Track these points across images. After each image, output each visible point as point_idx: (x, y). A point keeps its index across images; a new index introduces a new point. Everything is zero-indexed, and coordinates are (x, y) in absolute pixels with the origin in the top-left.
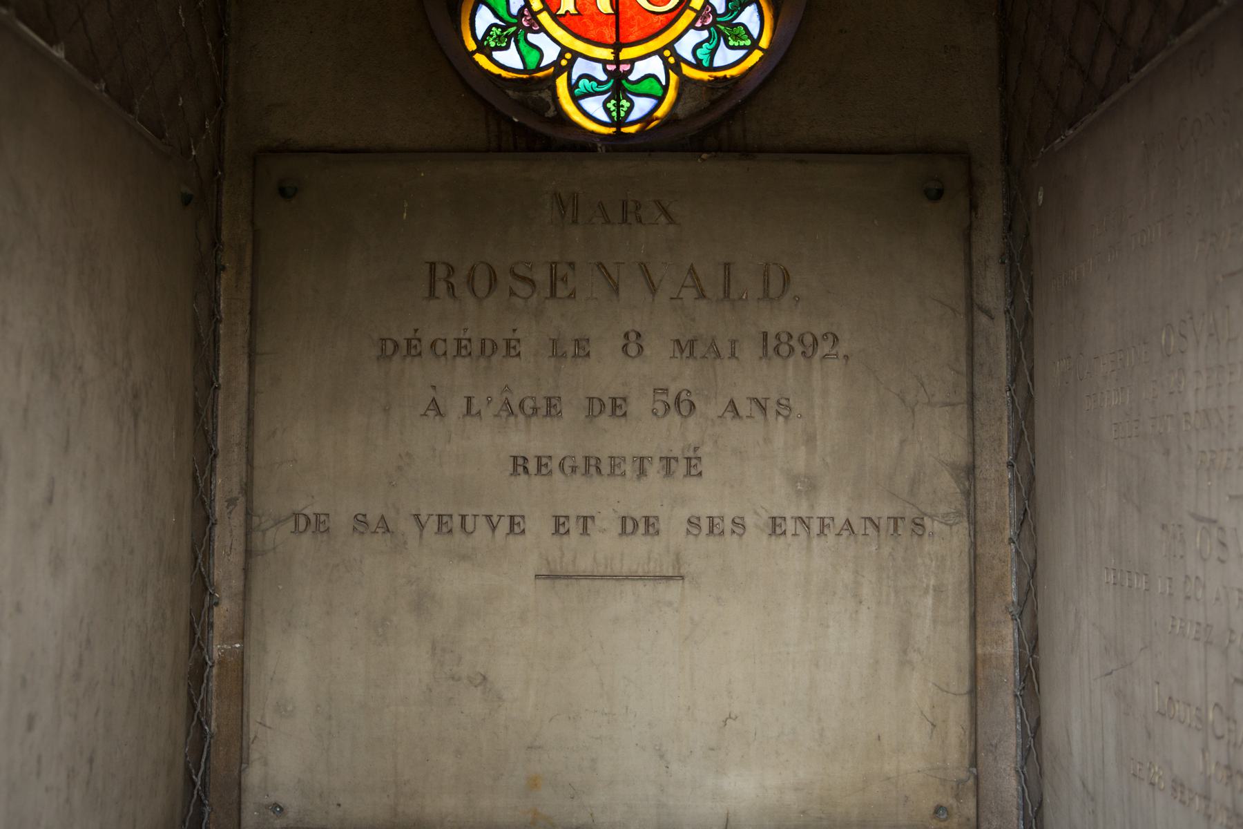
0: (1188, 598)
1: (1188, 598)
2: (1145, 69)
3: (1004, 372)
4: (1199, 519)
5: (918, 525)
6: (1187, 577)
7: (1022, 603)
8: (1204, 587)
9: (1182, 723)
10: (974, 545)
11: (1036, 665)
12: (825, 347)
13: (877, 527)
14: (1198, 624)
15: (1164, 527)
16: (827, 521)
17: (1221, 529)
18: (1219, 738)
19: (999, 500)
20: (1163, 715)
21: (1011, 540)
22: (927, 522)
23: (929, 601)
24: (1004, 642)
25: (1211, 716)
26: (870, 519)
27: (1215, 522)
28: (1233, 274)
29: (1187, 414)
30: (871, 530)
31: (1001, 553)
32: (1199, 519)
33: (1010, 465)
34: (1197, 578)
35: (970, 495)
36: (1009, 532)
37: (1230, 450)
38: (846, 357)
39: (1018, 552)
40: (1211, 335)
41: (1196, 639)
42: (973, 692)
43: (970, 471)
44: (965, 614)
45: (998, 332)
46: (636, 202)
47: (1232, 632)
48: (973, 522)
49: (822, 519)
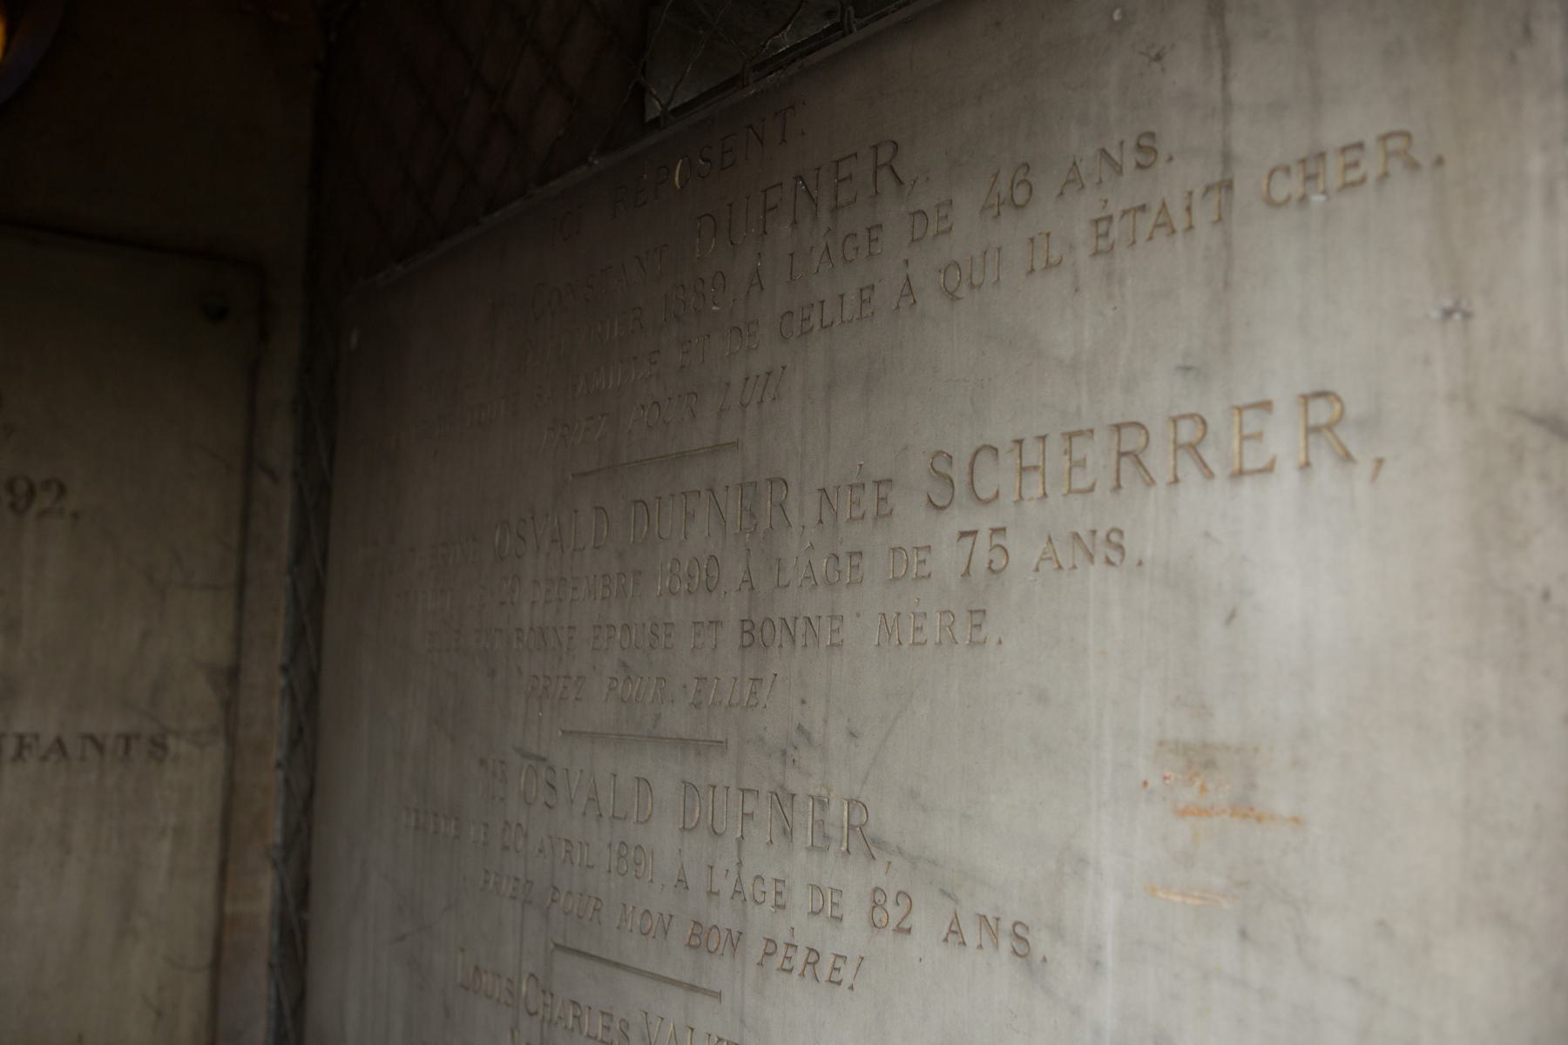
0: (506, 848)
1: (506, 848)
2: (497, 214)
3: (285, 550)
4: (526, 755)
5: (158, 747)
6: (506, 823)
7: (287, 847)
8: (526, 836)
9: (489, 997)
10: (230, 771)
11: (304, 928)
12: (45, 499)
13: (100, 748)
14: (517, 879)
15: (483, 762)
16: (27, 740)
17: (551, 768)
18: (531, 1014)
19: (267, 712)
20: (467, 989)
21: (279, 765)
22: (171, 742)
23: (166, 846)
24: (261, 896)
25: (524, 989)
26: (92, 738)
27: (544, 760)
28: (585, 474)
29: (519, 630)
30: (91, 752)
31: (266, 783)
32: (526, 755)
33: (285, 669)
34: (519, 825)
35: (229, 706)
36: (277, 753)
37: (567, 677)
38: (75, 515)
39: (287, 781)
40: (554, 541)
41: (514, 898)
42: (216, 966)
43: (233, 674)
44: (212, 863)
45: (280, 502)
46: (623, 1020)
47: (555, 888)
48: (231, 740)
49: (21, 738)
